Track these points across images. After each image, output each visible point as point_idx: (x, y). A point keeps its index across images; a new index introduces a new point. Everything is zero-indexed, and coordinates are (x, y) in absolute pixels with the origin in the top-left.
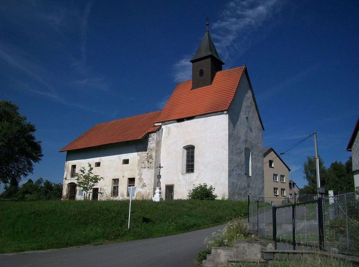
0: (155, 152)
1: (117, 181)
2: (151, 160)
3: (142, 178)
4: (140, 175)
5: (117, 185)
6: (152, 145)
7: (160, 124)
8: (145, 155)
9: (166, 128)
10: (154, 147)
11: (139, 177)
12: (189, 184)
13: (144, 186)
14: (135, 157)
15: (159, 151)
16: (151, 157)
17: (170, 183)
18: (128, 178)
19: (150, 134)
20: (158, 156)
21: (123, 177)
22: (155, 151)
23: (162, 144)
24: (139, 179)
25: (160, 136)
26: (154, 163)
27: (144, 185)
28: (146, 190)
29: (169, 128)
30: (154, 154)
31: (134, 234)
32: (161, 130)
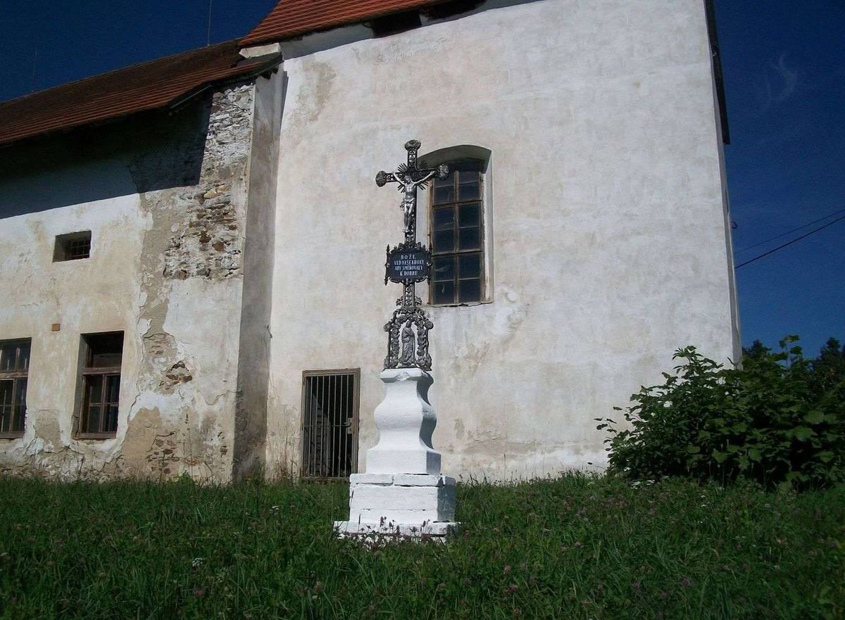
0: (244, 186)
1: (18, 350)
2: (220, 232)
3: (165, 334)
4: (156, 313)
5: (19, 375)
6: (232, 147)
7: (275, 48)
8: (186, 203)
9: (306, 70)
10: (243, 160)
11: (145, 326)
12: (457, 367)
13: (178, 376)
14: (126, 218)
15: (266, 184)
16: (222, 214)
17: (332, 362)
18: (82, 334)
19: (216, 95)
20: (261, 211)
21: (56, 327)
22: (246, 179)
23: (282, 151)
24: (145, 338)
25: (275, 105)
26: (239, 245)
27: (176, 372)
28: (188, 400)
29: (323, 66)
30: (240, 197)
31: (213, 191)
32: (277, 78)
